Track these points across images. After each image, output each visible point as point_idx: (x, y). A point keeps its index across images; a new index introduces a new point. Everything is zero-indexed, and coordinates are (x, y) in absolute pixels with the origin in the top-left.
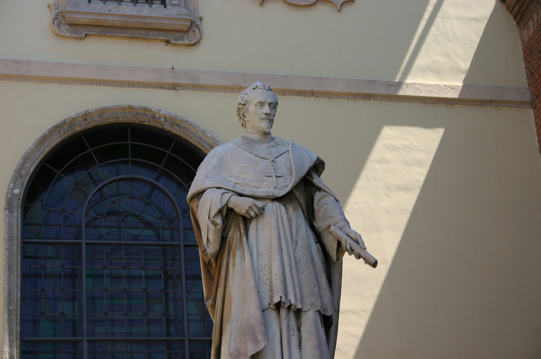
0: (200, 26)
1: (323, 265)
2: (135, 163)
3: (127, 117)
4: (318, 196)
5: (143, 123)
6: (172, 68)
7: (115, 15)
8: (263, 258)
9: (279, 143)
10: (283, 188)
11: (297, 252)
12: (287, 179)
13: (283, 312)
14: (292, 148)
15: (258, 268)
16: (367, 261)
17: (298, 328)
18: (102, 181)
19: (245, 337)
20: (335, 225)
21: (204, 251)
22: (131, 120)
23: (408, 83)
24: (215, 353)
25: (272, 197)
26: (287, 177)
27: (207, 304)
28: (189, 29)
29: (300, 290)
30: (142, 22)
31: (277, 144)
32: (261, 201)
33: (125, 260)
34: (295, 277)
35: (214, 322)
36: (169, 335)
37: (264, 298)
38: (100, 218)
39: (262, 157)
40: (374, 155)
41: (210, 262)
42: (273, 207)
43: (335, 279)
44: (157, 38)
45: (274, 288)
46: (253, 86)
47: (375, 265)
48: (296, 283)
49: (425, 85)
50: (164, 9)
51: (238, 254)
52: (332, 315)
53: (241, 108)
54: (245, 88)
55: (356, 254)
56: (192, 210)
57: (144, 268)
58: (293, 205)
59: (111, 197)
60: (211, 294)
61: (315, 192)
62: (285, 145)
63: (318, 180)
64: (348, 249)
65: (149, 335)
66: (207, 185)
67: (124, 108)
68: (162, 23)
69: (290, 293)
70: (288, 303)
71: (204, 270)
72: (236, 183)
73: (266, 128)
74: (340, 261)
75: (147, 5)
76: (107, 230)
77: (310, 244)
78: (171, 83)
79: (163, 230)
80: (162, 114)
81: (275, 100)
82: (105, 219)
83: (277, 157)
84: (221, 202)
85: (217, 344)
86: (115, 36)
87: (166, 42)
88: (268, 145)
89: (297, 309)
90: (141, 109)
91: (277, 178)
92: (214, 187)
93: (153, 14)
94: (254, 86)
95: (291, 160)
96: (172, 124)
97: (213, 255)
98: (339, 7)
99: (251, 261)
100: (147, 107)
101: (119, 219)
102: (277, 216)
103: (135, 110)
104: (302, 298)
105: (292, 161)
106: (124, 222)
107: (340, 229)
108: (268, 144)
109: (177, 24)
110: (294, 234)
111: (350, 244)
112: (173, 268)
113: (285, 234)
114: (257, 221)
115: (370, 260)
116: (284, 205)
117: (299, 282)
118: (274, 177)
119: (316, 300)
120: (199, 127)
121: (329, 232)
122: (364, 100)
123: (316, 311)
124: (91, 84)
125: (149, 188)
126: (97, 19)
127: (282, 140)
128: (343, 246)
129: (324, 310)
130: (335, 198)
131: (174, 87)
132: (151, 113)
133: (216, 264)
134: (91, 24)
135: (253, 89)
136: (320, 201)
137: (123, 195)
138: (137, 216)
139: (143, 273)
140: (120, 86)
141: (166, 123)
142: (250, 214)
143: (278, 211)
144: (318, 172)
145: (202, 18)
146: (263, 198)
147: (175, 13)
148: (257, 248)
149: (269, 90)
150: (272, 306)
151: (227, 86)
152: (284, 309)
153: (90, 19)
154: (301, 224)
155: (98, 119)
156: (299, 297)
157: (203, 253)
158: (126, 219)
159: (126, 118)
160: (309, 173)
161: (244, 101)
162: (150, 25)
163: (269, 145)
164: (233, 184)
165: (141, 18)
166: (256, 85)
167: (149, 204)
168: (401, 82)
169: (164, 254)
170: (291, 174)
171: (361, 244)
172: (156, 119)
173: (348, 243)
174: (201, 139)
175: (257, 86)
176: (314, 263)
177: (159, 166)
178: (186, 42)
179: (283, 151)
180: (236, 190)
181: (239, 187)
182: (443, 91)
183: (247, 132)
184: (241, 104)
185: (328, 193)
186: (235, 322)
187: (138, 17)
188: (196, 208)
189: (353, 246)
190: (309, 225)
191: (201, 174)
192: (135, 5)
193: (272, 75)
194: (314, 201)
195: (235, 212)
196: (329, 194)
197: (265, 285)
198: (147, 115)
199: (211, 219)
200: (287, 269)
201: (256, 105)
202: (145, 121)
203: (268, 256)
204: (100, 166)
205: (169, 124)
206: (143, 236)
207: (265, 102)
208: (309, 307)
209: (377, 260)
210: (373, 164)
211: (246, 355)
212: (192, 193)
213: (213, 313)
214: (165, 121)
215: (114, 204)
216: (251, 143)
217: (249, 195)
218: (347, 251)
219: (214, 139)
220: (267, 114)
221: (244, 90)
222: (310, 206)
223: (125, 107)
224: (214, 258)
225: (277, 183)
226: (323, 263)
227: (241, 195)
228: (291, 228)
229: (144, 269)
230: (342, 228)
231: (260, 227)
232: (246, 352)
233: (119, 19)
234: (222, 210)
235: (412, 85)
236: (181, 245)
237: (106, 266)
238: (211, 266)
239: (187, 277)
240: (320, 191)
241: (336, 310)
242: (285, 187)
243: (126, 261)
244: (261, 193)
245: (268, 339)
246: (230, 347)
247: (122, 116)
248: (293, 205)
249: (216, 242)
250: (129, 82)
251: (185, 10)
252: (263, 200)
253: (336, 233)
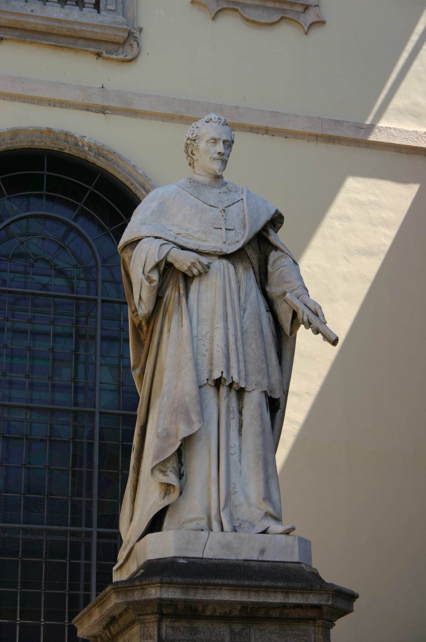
0: (139, 39)
1: (274, 338)
2: (50, 199)
3: (45, 141)
4: (273, 255)
5: (62, 151)
6: (101, 86)
7: (38, 17)
8: (204, 325)
9: (232, 190)
10: (234, 243)
11: (244, 320)
12: (239, 233)
13: (223, 390)
14: (247, 197)
15: (197, 337)
16: (326, 338)
17: (239, 410)
18: (8, 216)
19: (176, 416)
20: (291, 292)
21: (136, 310)
22: (49, 146)
23: (381, 127)
24: (139, 433)
25: (220, 254)
26: (239, 231)
27: (133, 373)
28: (126, 41)
29: (245, 366)
30: (70, 28)
31: (230, 191)
32: (207, 257)
33: (31, 312)
34: (241, 350)
35: (141, 396)
36: (76, 404)
37: (201, 372)
38: (4, 260)
39: (211, 205)
40: (335, 210)
41: (140, 325)
42: (220, 265)
43: (286, 355)
44: (86, 49)
45: (215, 362)
46: (206, 118)
47: (335, 343)
48: (241, 357)
49: (400, 131)
50: (97, 14)
51: (175, 318)
52: (279, 398)
53: (190, 144)
54: (196, 120)
55: (314, 328)
56: (124, 261)
57: (53, 323)
58: (244, 264)
59: (19, 237)
60: (140, 362)
61: (271, 251)
62: (239, 193)
63: (275, 237)
64: (305, 322)
65: (53, 402)
66: (143, 233)
67: (41, 131)
68: (93, 32)
69: (232, 368)
70: (230, 380)
71: (133, 333)
72: (178, 234)
73: (217, 170)
74: (293, 335)
75: (77, 8)
76: (12, 275)
77: (260, 312)
78: (99, 105)
79: (78, 280)
80: (87, 142)
81: (231, 137)
82: (10, 262)
83: (229, 206)
84: (158, 255)
85: (142, 422)
86: (37, 43)
87: (97, 54)
88: (219, 191)
89: (240, 388)
90: (61, 133)
91: (228, 231)
92: (152, 236)
93: (84, 20)
94: (208, 119)
95: (245, 210)
96: (98, 154)
97: (145, 316)
98: (306, 28)
99: (190, 328)
100: (69, 132)
101: (26, 262)
102: (224, 276)
103: (55, 134)
104: (246, 375)
105: (246, 212)
106: (32, 267)
107: (297, 297)
108: (219, 190)
109: (111, 35)
110: (243, 300)
111: (307, 316)
112: (87, 326)
113: (233, 299)
114: (200, 281)
115: (329, 336)
116: (233, 264)
117: (244, 356)
118: (224, 229)
119: (263, 379)
120: (129, 161)
121: (284, 301)
122: (328, 143)
123: (261, 392)
124: (4, 99)
125: (63, 229)
126: (15, 20)
127: (236, 186)
128: (298, 318)
129: (271, 391)
130: (293, 260)
131: (103, 111)
132: (74, 139)
133: (148, 327)
134: (8, 26)
135: (206, 122)
136: (276, 263)
137: (34, 235)
138: (49, 261)
139: (51, 329)
140: (38, 104)
141: (90, 153)
142: (192, 272)
143: (226, 270)
144: (275, 227)
145: (142, 29)
146: (209, 253)
147: (109, 20)
148: (198, 313)
149: (225, 125)
150: (210, 382)
151: (166, 114)
152: (225, 387)
153: (7, 19)
154: (252, 287)
155: (9, 141)
156: (243, 374)
157: (133, 313)
158: (35, 264)
159: (43, 143)
160: (265, 228)
161: (194, 135)
162: (79, 33)
163: (220, 190)
164: (174, 234)
165: (69, 23)
166: (209, 117)
167: (64, 249)
168: (373, 125)
169: (78, 309)
170: (244, 227)
171: (321, 317)
172: (79, 148)
173: (305, 315)
174: (130, 176)
175: (211, 119)
176: (263, 336)
177: (79, 204)
178: (121, 57)
179: (236, 199)
180: (177, 241)
181: (182, 239)
182: (422, 139)
183: (195, 173)
184: (190, 139)
185: (286, 253)
186: (166, 397)
187: (66, 22)
188: (129, 259)
189: (311, 319)
190: (261, 290)
191: (137, 220)
192: (63, 7)
193: (221, 105)
194: (269, 261)
195: (175, 268)
196: (287, 254)
197: (205, 356)
198: (68, 141)
199: (145, 274)
200: (232, 339)
201: (207, 142)
202: (65, 149)
203: (210, 323)
204: (9, 199)
205: (94, 154)
206: (54, 285)
207: (219, 139)
208: (254, 387)
209: (338, 338)
210: (332, 221)
211: (177, 437)
212: (125, 242)
213: (140, 386)
214: (89, 150)
215: (21, 245)
216: (199, 187)
217: (192, 249)
218: (303, 324)
219: (146, 176)
220: (220, 154)
221: (195, 123)
222: (263, 267)
223: (43, 129)
224: (145, 320)
225: (226, 237)
226: (273, 336)
227: (183, 248)
228: (239, 292)
229: (53, 325)
230: (300, 296)
231: (203, 287)
232: (177, 433)
233: (42, 23)
234: (160, 265)
235: (386, 129)
236: (98, 300)
237: (7, 318)
238: (141, 329)
239: (104, 338)
240: (276, 251)
241: (285, 392)
242: (236, 242)
243: (32, 314)
244: (207, 247)
245: (204, 420)
246: (157, 427)
247: (39, 140)
248: (244, 264)
249: (149, 301)
250: (49, 100)
251: (123, 18)
252: (209, 256)
253: (292, 302)
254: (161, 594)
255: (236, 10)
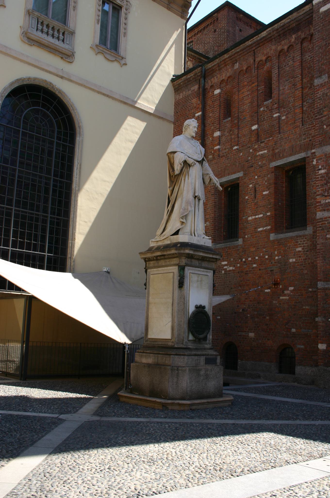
178: (69, 60)
254: (80, 233)
255: (103, 54)
